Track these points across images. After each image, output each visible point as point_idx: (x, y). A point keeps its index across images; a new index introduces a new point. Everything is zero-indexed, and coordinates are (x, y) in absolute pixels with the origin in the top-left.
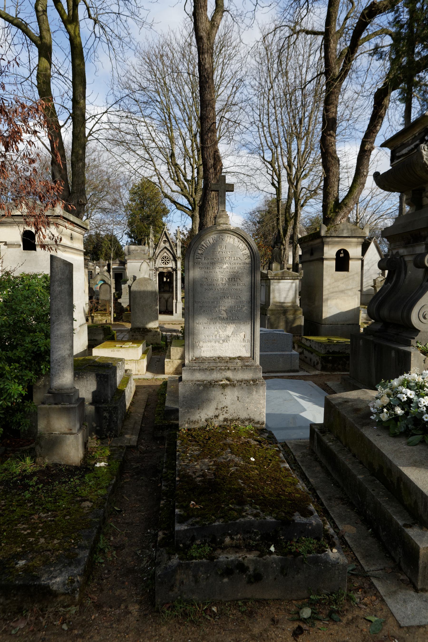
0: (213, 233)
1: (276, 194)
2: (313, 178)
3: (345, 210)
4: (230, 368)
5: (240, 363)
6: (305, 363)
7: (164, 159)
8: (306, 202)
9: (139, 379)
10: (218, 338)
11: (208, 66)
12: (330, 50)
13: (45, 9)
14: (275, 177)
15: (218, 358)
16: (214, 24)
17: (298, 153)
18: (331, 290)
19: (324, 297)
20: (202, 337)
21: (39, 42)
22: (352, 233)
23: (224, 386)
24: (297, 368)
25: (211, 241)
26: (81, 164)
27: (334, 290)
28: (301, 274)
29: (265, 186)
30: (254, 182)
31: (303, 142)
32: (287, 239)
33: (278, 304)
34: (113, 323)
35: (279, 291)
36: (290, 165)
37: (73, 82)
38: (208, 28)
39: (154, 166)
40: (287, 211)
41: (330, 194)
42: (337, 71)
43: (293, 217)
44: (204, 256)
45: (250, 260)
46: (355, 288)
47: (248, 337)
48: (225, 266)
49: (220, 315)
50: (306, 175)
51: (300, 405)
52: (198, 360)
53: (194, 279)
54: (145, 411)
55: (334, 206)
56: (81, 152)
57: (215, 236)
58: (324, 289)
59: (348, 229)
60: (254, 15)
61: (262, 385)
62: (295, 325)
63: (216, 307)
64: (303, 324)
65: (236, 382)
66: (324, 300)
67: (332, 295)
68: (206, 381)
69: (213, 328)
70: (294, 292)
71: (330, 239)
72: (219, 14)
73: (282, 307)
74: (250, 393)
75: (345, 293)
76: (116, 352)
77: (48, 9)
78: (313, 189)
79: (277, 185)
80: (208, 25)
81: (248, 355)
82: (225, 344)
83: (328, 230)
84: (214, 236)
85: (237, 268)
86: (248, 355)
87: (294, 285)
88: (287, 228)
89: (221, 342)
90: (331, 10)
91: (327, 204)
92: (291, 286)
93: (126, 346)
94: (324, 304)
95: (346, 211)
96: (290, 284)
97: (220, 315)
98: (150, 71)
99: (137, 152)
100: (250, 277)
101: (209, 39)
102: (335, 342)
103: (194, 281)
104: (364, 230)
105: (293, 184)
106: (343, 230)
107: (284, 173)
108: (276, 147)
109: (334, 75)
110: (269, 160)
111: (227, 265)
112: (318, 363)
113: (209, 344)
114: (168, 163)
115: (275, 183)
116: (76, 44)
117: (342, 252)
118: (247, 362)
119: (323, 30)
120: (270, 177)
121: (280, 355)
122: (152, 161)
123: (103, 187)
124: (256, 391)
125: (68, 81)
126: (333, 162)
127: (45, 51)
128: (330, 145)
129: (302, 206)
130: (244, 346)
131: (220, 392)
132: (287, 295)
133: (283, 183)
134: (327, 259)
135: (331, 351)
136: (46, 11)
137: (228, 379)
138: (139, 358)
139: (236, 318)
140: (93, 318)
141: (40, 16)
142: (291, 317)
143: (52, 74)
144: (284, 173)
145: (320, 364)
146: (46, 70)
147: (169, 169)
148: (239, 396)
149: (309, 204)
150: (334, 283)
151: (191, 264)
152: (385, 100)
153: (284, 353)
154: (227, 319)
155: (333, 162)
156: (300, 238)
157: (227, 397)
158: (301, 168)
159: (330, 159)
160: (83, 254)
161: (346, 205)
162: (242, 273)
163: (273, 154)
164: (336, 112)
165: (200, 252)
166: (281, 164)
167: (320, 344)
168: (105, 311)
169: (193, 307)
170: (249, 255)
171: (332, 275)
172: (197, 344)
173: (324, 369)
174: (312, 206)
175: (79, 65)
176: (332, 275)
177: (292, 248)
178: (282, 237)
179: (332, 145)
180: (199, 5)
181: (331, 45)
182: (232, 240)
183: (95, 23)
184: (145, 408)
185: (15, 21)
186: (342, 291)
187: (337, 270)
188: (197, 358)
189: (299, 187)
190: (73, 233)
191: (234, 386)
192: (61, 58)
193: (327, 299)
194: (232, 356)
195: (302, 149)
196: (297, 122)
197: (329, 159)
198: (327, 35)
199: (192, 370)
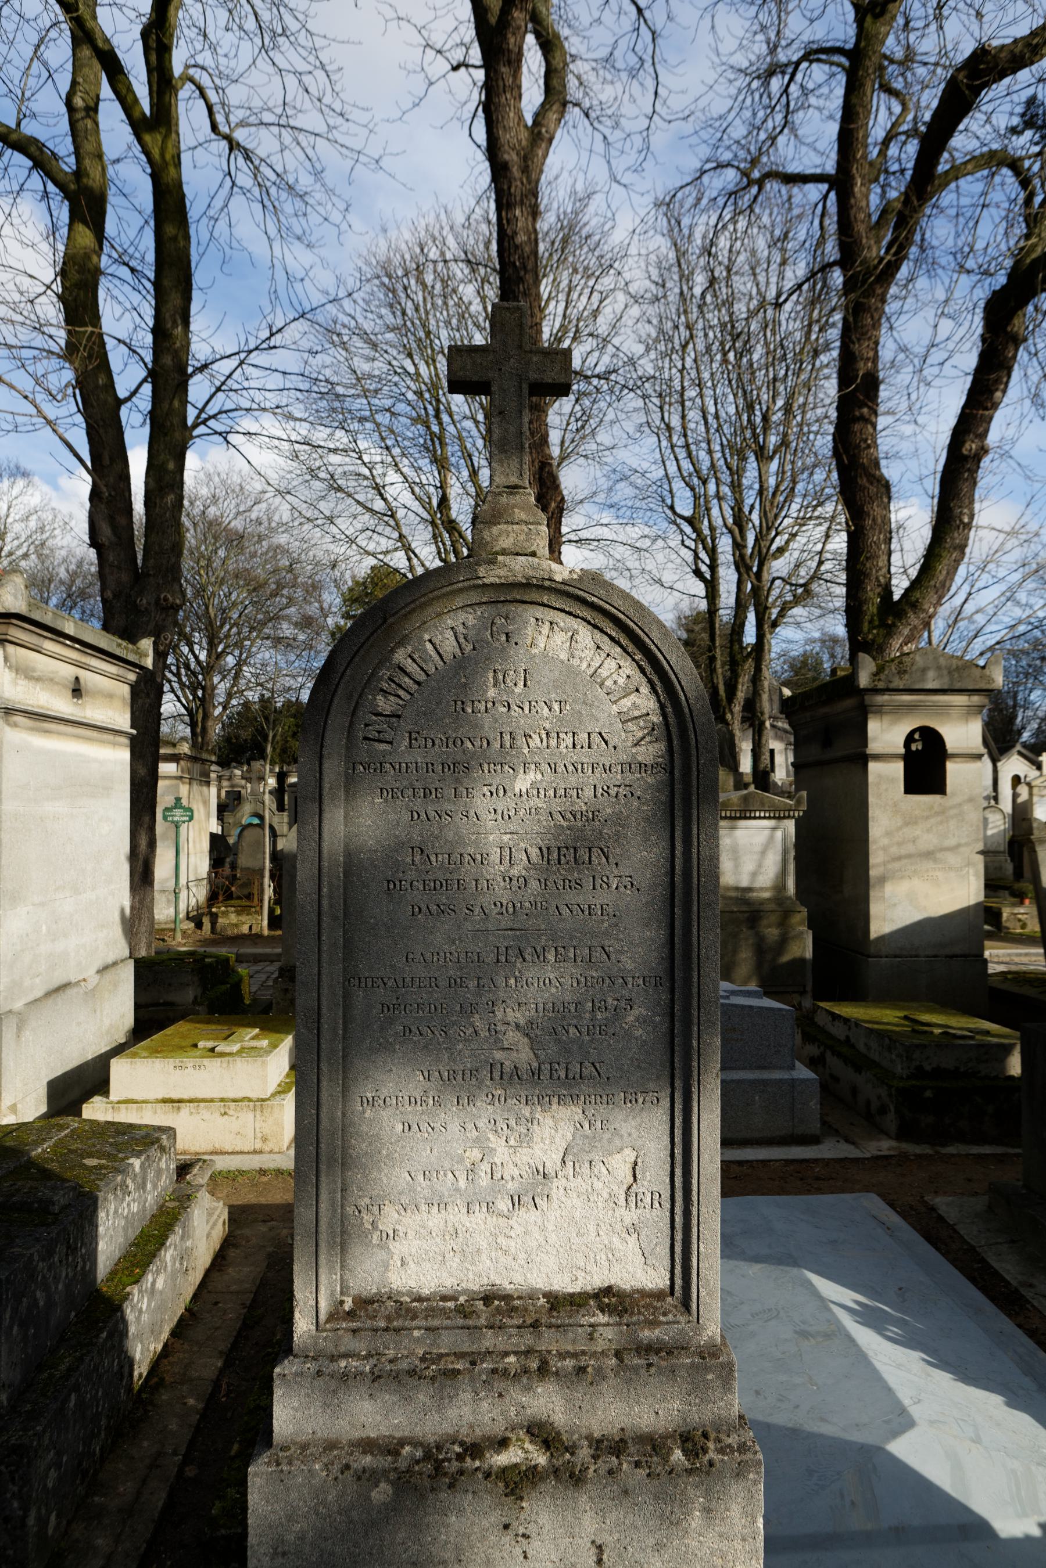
0: (459, 601)
1: (707, 597)
2: (814, 541)
3: (914, 620)
4: (555, 1364)
5: (609, 1333)
6: (842, 1107)
7: (425, 515)
8: (783, 616)
9: (262, 1172)
10: (484, 1181)
11: (525, 238)
12: (852, 201)
13: (92, 104)
14: (703, 555)
15: (487, 1299)
16: (540, 133)
17: (761, 492)
18: (894, 850)
19: (872, 873)
20: (395, 1177)
21: (73, 187)
22: (952, 679)
23: (517, 1483)
24: (814, 1126)
25: (449, 645)
26: (170, 498)
27: (903, 852)
28: (799, 802)
29: (676, 578)
30: (650, 565)
31: (774, 466)
32: (737, 708)
33: (733, 894)
34: (266, 932)
35: (735, 851)
36: (740, 520)
37: (157, 284)
38: (524, 143)
39: (397, 527)
40: (736, 637)
41: (867, 575)
42: (876, 250)
43: (750, 654)
44: (406, 726)
45: (660, 747)
46: (967, 844)
47: (656, 1177)
48: (522, 783)
49: (498, 1055)
50: (781, 551)
51: (876, 1377)
52: (365, 1310)
53: (348, 855)
54: (228, 1364)
55: (879, 608)
56: (171, 466)
57: (471, 621)
58: (872, 847)
59: (939, 668)
60: (646, 140)
61: (739, 1474)
62: (785, 958)
63: (473, 1008)
64: (809, 954)
65: (584, 1452)
66: (872, 881)
67: (896, 865)
68: (415, 1443)
69: (454, 1127)
70: (779, 858)
71: (886, 697)
72: (555, 108)
73: (747, 902)
74: (671, 1521)
75: (935, 861)
76: (190, 1070)
77: (101, 105)
78: (802, 581)
79: (708, 577)
80: (524, 135)
81: (654, 1277)
82: (526, 1216)
83: (880, 670)
84: (462, 616)
85: (588, 793)
86: (654, 1277)
87: (779, 834)
88: (736, 682)
89: (503, 1205)
90: (854, 100)
91: (861, 605)
92: (771, 839)
93: (228, 1049)
94: (873, 894)
95: (916, 622)
96: (767, 832)
97: (498, 1055)
98: (391, 306)
99: (356, 496)
100: (664, 844)
101: (525, 170)
102: (937, 1031)
103: (353, 865)
104: (987, 671)
105: (751, 568)
106: (924, 670)
107: (725, 545)
108: (705, 482)
109: (862, 276)
110: (688, 513)
111: (532, 776)
112: (883, 1110)
113: (435, 1220)
114: (433, 523)
115: (704, 568)
116: (167, 185)
117: (917, 736)
118: (653, 1324)
119: (830, 167)
120: (689, 556)
121: (753, 1082)
122: (392, 516)
123: (280, 586)
124: (707, 1510)
125: (144, 281)
126: (873, 490)
127: (86, 202)
128: (863, 445)
129: (775, 624)
130: (634, 1229)
131: (496, 1518)
132: (760, 866)
133: (722, 571)
134: (877, 757)
135: (928, 1068)
136: (96, 110)
137: (543, 1433)
138: (272, 1087)
139: (589, 1070)
140: (214, 918)
141: (78, 121)
142: (772, 933)
143: (103, 265)
144: (725, 545)
145: (891, 1116)
146: (87, 257)
147: (435, 537)
148: (608, 1539)
149: (791, 620)
150: (899, 829)
151: (333, 769)
152: (1016, 321)
153: (766, 1075)
154: (535, 1074)
155: (873, 490)
156: (789, 698)
157: (535, 1547)
158: (769, 529)
159: (863, 481)
160: (127, 741)
161: (915, 606)
162: (619, 820)
163: (696, 498)
164: (876, 359)
165: (384, 704)
166: (718, 522)
167: (884, 1037)
168: (248, 900)
169: (347, 1008)
170: (656, 718)
171: (895, 805)
172: (367, 1218)
173: (904, 1133)
174: (798, 624)
175: (174, 239)
176: (895, 805)
177: (750, 731)
178: (724, 703)
179: (869, 447)
180: (501, 83)
181: (856, 189)
182: (559, 639)
183: (231, 150)
184: (234, 1346)
185: (14, 137)
186: (929, 855)
187: (907, 791)
188: (364, 1303)
189: (766, 577)
190: (83, 674)
191: (576, 1479)
192: (129, 221)
193: (883, 880)
194: (565, 1284)
195: (772, 481)
196: (758, 420)
197: (861, 487)
198: (841, 182)
199: (335, 1379)
